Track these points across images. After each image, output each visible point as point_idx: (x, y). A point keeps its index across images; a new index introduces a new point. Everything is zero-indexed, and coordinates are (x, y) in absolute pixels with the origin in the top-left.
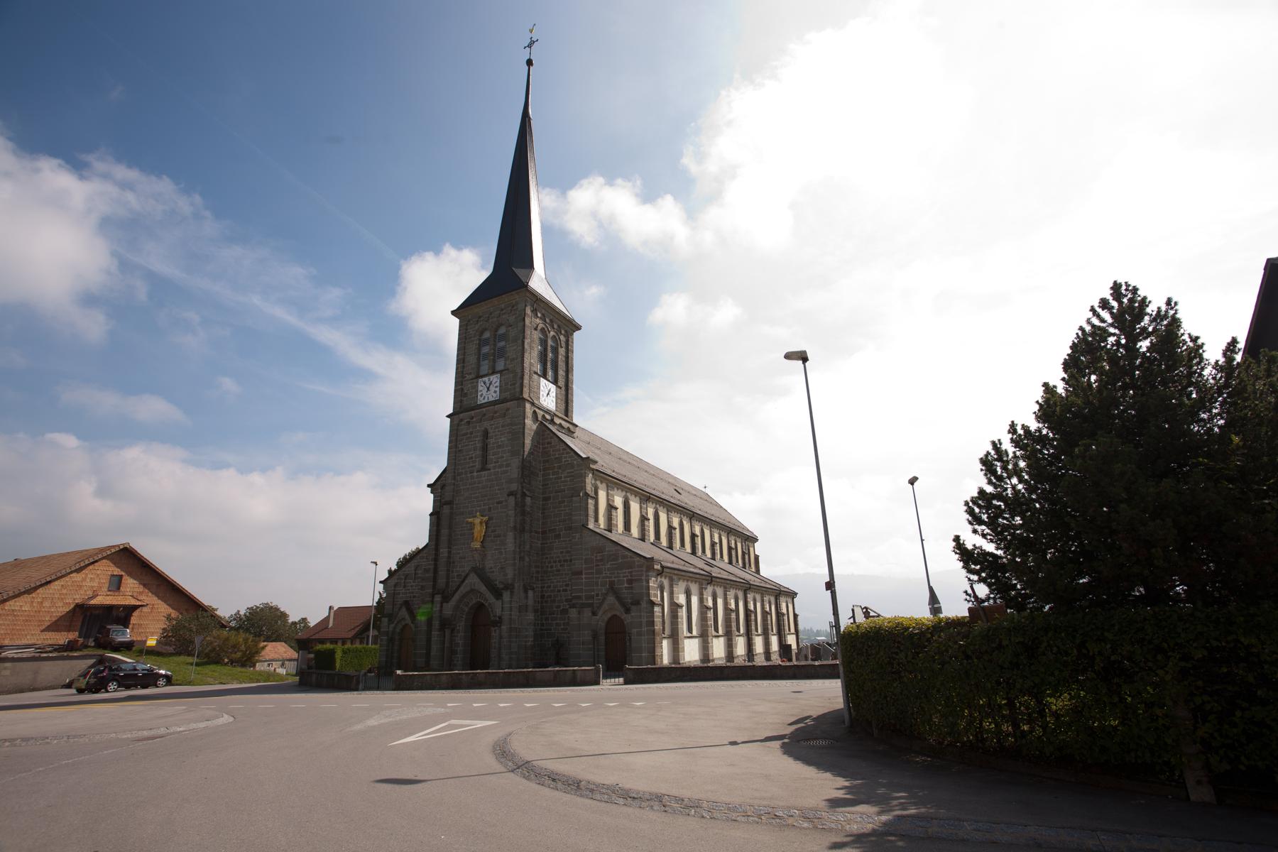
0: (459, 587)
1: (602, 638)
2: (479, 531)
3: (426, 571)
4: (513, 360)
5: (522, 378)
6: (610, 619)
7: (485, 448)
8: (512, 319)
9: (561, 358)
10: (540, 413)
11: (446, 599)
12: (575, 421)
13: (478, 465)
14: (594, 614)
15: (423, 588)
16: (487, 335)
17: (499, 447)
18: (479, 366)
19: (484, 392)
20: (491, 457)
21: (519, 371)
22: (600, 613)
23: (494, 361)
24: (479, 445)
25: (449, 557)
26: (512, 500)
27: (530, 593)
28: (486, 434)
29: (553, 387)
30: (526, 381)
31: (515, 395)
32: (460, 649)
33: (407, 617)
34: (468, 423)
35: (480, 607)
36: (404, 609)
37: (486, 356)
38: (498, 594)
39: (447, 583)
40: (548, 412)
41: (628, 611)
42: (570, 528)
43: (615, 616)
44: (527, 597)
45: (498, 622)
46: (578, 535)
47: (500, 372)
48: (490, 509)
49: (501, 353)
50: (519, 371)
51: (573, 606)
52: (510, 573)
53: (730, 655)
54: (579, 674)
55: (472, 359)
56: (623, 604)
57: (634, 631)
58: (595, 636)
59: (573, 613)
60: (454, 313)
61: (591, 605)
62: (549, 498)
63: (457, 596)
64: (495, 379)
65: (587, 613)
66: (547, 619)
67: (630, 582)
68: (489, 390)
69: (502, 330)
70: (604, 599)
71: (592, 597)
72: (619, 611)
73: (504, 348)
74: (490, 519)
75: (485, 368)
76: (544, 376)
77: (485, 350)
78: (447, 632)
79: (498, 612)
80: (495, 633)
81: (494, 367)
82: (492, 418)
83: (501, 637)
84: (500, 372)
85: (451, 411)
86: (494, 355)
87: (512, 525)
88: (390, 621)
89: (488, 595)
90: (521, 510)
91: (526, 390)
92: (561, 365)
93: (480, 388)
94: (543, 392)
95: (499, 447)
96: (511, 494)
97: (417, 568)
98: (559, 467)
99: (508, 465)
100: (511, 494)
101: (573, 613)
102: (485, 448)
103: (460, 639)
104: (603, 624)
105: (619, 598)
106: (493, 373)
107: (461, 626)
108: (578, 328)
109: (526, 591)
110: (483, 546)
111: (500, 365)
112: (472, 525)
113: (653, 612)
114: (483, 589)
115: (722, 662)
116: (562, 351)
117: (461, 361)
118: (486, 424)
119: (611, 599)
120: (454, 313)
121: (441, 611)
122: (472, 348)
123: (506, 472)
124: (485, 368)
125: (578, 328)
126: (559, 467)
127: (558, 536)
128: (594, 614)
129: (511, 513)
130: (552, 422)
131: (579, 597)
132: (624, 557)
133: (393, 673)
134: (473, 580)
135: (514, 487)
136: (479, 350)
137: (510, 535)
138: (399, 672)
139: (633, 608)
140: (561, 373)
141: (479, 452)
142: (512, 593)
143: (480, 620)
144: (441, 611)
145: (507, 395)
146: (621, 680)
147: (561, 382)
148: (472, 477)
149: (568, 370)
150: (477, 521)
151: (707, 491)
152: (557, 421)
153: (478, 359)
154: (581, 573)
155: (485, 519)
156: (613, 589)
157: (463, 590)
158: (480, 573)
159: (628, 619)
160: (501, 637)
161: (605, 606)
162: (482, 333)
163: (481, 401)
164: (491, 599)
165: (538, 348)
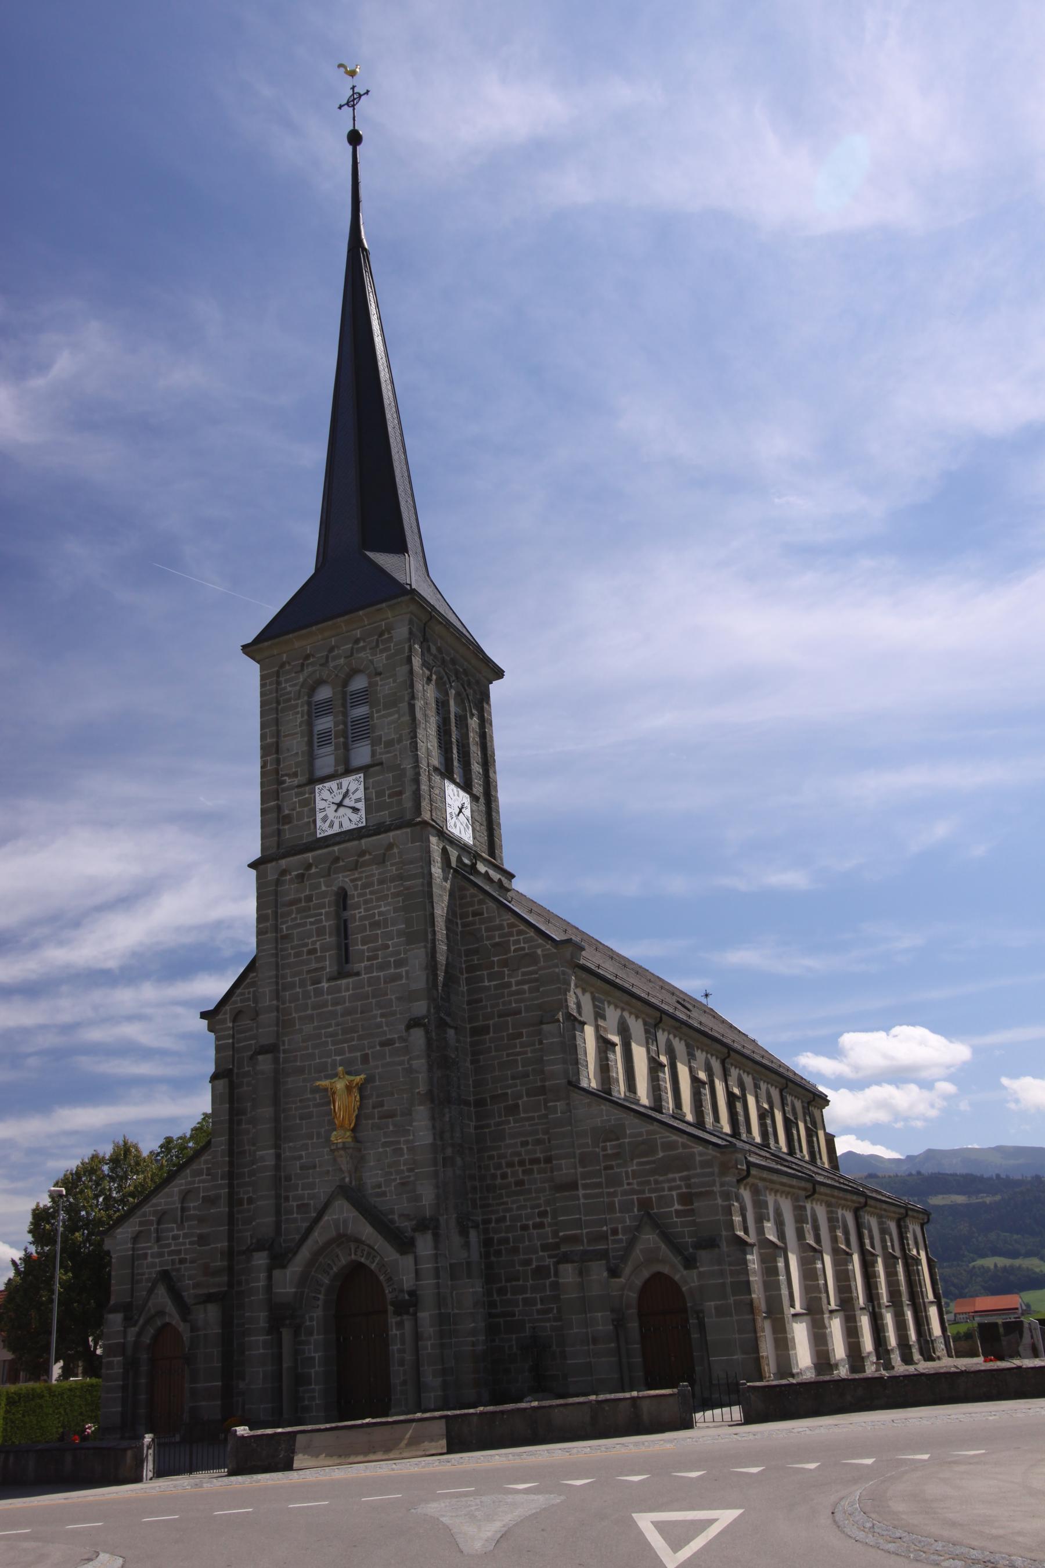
0: (309, 1230)
1: (634, 1325)
2: (344, 1105)
3: (210, 1201)
4: (390, 744)
5: (417, 781)
6: (647, 1283)
7: (343, 930)
8: (380, 660)
9: (473, 737)
10: (454, 854)
11: (279, 1259)
12: (507, 866)
13: (329, 966)
14: (614, 1273)
15: (203, 1240)
16: (324, 693)
17: (375, 925)
18: (311, 757)
19: (330, 812)
20: (358, 947)
21: (407, 765)
22: (628, 1270)
23: (346, 748)
24: (328, 924)
25: (277, 1167)
26: (418, 1036)
27: (473, 1235)
28: (342, 898)
29: (464, 798)
30: (424, 787)
31: (401, 814)
32: (316, 1370)
33: (170, 1307)
34: (301, 877)
35: (356, 1274)
36: (161, 1290)
37: (325, 738)
38: (404, 1245)
39: (278, 1224)
40: (463, 848)
41: (690, 1263)
42: (542, 1091)
43: (658, 1276)
44: (467, 1245)
45: (409, 1305)
46: (560, 1105)
47: (364, 769)
48: (365, 1059)
49: (363, 730)
50: (407, 765)
51: (565, 1259)
52: (427, 1194)
53: (823, 1360)
54: (645, 1406)
55: (295, 745)
56: (677, 1248)
57: (711, 1305)
58: (619, 1323)
59: (568, 1274)
60: (247, 649)
61: (604, 1255)
62: (485, 1030)
63: (305, 1253)
64: (355, 784)
65: (598, 1272)
66: (502, 1291)
67: (686, 1199)
68: (338, 807)
69: (359, 683)
70: (632, 1242)
71: (603, 1237)
72: (672, 1266)
73: (369, 717)
74: (369, 1080)
75: (326, 761)
76: (447, 773)
77: (325, 723)
78: (286, 1334)
79: (407, 1281)
80: (398, 1332)
81: (346, 761)
82: (356, 866)
83: (417, 1337)
84: (364, 769)
85: (256, 853)
86: (344, 734)
87: (422, 1088)
88: (129, 1321)
89: (379, 1242)
90: (440, 1058)
91: (425, 804)
92: (475, 751)
93: (320, 804)
94: (452, 808)
95: (375, 925)
96: (414, 1023)
97: (185, 1196)
98: (505, 963)
99: (399, 964)
100: (414, 1023)
101: (568, 1274)
102: (343, 930)
103: (315, 1350)
104: (634, 1295)
105: (667, 1237)
106: (348, 771)
107: (315, 1316)
108: (499, 674)
109: (464, 1232)
110: (356, 1140)
111: (362, 754)
112: (328, 1096)
113: (745, 1262)
114: (367, 1231)
115: (810, 1376)
116: (474, 723)
117: (271, 749)
118: (343, 879)
119: (649, 1238)
120: (247, 649)
121: (269, 1288)
122: (293, 721)
123: (397, 977)
124: (326, 761)
125: (499, 674)
126: (505, 963)
127: (513, 1109)
128: (614, 1273)
129: (420, 1063)
130: (473, 868)
131: (575, 1239)
132: (669, 1146)
133: (228, 1432)
134: (342, 1212)
135: (420, 1008)
136: (310, 724)
137: (421, 1114)
138: (242, 1430)
139: (703, 1255)
140: (476, 768)
141: (329, 939)
142: (436, 1236)
143: (357, 1300)
144: (269, 1288)
145: (385, 816)
146: (736, 1413)
147: (478, 790)
148: (318, 992)
149: (487, 762)
150: (340, 1085)
151: (711, 1003)
152: (482, 868)
153: (310, 743)
154: (573, 1186)
155: (358, 1079)
156: (649, 1216)
157: (318, 1237)
158: (353, 1194)
159: (689, 1280)
160: (417, 1337)
161: (637, 1253)
162: (312, 690)
163: (324, 830)
164: (390, 1254)
165: (433, 721)
